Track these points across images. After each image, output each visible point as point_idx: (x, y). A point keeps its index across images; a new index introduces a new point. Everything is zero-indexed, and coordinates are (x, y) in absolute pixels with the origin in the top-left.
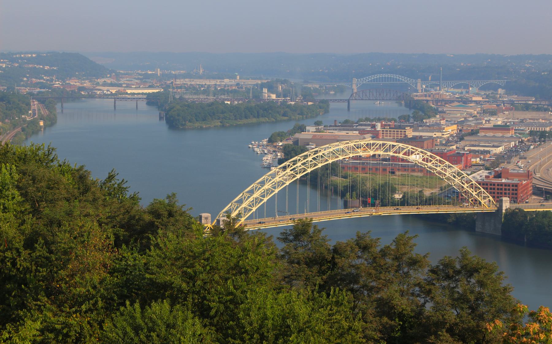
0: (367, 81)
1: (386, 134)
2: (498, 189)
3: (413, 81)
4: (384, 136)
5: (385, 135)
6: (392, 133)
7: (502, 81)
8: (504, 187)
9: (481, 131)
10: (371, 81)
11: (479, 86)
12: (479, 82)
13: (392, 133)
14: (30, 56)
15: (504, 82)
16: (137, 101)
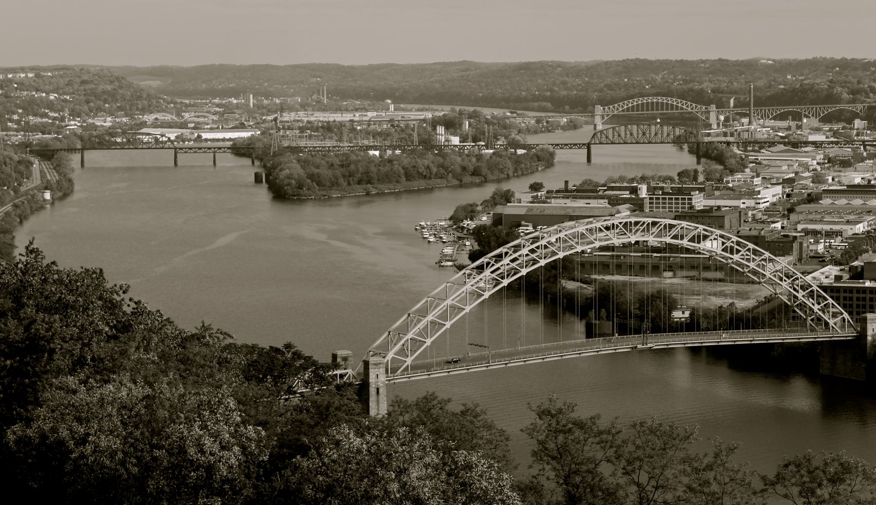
8: (855, 295)
9: (826, 195)
10: (628, 110)
11: (820, 115)
16: (214, 153)
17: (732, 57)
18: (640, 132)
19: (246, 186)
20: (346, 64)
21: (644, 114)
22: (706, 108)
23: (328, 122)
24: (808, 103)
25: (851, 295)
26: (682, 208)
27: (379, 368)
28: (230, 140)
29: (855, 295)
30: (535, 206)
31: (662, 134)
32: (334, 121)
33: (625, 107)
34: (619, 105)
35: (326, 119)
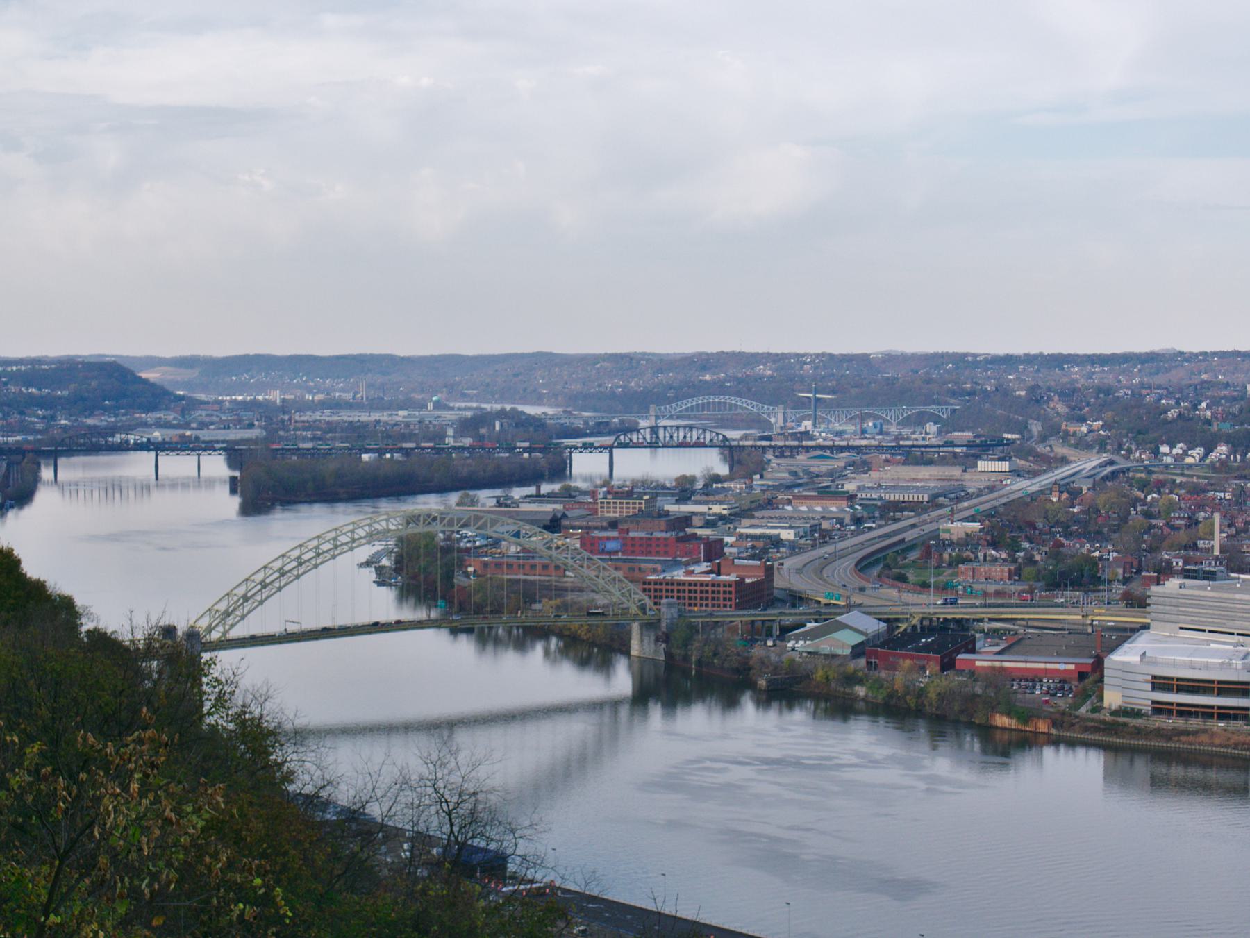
1: (608, 508)
6: (605, 505)
8: (664, 587)
11: (898, 418)
12: (843, 411)
13: (605, 505)
14: (14, 368)
19: (224, 523)
20: (1109, 353)
23: (351, 422)
25: (690, 595)
26: (627, 512)
28: (1140, 623)
30: (662, 556)
33: (684, 407)
34: (677, 405)
35: (351, 419)
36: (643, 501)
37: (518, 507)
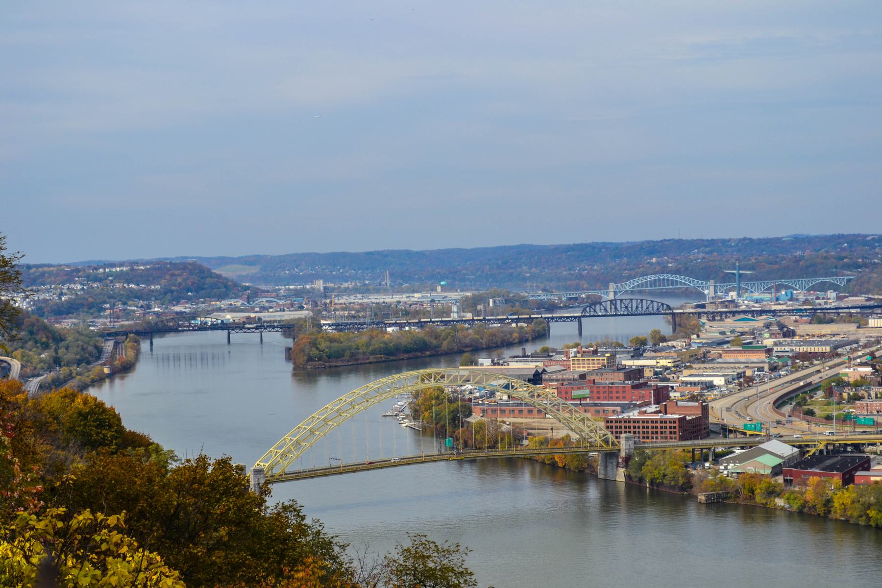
0: (632, 286)
2: (653, 427)
3: (702, 283)
4: (574, 367)
5: (591, 365)
7: (840, 279)
8: (623, 425)
9: (725, 355)
10: (638, 286)
15: (843, 279)
17: (755, 237)
18: (623, 306)
21: (679, 288)
22: (706, 284)
24: (459, 290)
27: (260, 474)
29: (668, 425)
31: (642, 307)
32: (384, 302)
35: (378, 301)
36: (605, 358)
37: (508, 365)
